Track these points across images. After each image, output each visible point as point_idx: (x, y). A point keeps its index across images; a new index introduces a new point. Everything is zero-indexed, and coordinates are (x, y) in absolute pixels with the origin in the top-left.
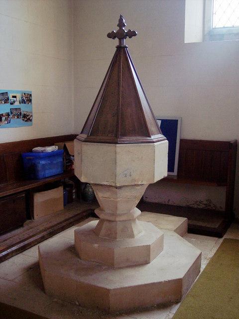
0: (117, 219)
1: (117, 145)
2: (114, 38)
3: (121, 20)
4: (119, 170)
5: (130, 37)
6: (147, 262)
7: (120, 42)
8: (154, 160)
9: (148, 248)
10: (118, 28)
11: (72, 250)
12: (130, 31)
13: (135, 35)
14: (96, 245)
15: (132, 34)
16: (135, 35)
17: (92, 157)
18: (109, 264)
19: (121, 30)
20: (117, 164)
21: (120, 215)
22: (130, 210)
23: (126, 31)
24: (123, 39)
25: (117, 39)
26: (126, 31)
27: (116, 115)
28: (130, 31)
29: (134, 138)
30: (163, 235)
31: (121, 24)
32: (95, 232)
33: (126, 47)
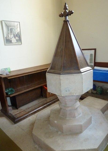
0: (66, 109)
1: (61, 75)
2: (63, 16)
3: (65, 6)
4: (62, 88)
5: (70, 15)
6: (81, 132)
7: (65, 18)
8: (84, 79)
9: (81, 126)
10: (64, 10)
11: (48, 119)
12: (69, 11)
13: (72, 13)
14: (56, 122)
15: (71, 13)
16: (72, 13)
17: (50, 81)
18: (60, 132)
19: (65, 12)
20: (61, 86)
21: (68, 107)
22: (50, 124)
23: (67, 12)
24: (66, 16)
25: (64, 17)
26: (67, 12)
27: (65, 58)
28: (69, 11)
29: (72, 71)
30: (91, 117)
31: (65, 8)
32: (59, 111)
33: (68, 21)
